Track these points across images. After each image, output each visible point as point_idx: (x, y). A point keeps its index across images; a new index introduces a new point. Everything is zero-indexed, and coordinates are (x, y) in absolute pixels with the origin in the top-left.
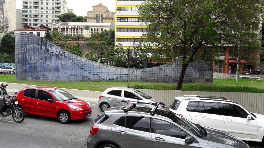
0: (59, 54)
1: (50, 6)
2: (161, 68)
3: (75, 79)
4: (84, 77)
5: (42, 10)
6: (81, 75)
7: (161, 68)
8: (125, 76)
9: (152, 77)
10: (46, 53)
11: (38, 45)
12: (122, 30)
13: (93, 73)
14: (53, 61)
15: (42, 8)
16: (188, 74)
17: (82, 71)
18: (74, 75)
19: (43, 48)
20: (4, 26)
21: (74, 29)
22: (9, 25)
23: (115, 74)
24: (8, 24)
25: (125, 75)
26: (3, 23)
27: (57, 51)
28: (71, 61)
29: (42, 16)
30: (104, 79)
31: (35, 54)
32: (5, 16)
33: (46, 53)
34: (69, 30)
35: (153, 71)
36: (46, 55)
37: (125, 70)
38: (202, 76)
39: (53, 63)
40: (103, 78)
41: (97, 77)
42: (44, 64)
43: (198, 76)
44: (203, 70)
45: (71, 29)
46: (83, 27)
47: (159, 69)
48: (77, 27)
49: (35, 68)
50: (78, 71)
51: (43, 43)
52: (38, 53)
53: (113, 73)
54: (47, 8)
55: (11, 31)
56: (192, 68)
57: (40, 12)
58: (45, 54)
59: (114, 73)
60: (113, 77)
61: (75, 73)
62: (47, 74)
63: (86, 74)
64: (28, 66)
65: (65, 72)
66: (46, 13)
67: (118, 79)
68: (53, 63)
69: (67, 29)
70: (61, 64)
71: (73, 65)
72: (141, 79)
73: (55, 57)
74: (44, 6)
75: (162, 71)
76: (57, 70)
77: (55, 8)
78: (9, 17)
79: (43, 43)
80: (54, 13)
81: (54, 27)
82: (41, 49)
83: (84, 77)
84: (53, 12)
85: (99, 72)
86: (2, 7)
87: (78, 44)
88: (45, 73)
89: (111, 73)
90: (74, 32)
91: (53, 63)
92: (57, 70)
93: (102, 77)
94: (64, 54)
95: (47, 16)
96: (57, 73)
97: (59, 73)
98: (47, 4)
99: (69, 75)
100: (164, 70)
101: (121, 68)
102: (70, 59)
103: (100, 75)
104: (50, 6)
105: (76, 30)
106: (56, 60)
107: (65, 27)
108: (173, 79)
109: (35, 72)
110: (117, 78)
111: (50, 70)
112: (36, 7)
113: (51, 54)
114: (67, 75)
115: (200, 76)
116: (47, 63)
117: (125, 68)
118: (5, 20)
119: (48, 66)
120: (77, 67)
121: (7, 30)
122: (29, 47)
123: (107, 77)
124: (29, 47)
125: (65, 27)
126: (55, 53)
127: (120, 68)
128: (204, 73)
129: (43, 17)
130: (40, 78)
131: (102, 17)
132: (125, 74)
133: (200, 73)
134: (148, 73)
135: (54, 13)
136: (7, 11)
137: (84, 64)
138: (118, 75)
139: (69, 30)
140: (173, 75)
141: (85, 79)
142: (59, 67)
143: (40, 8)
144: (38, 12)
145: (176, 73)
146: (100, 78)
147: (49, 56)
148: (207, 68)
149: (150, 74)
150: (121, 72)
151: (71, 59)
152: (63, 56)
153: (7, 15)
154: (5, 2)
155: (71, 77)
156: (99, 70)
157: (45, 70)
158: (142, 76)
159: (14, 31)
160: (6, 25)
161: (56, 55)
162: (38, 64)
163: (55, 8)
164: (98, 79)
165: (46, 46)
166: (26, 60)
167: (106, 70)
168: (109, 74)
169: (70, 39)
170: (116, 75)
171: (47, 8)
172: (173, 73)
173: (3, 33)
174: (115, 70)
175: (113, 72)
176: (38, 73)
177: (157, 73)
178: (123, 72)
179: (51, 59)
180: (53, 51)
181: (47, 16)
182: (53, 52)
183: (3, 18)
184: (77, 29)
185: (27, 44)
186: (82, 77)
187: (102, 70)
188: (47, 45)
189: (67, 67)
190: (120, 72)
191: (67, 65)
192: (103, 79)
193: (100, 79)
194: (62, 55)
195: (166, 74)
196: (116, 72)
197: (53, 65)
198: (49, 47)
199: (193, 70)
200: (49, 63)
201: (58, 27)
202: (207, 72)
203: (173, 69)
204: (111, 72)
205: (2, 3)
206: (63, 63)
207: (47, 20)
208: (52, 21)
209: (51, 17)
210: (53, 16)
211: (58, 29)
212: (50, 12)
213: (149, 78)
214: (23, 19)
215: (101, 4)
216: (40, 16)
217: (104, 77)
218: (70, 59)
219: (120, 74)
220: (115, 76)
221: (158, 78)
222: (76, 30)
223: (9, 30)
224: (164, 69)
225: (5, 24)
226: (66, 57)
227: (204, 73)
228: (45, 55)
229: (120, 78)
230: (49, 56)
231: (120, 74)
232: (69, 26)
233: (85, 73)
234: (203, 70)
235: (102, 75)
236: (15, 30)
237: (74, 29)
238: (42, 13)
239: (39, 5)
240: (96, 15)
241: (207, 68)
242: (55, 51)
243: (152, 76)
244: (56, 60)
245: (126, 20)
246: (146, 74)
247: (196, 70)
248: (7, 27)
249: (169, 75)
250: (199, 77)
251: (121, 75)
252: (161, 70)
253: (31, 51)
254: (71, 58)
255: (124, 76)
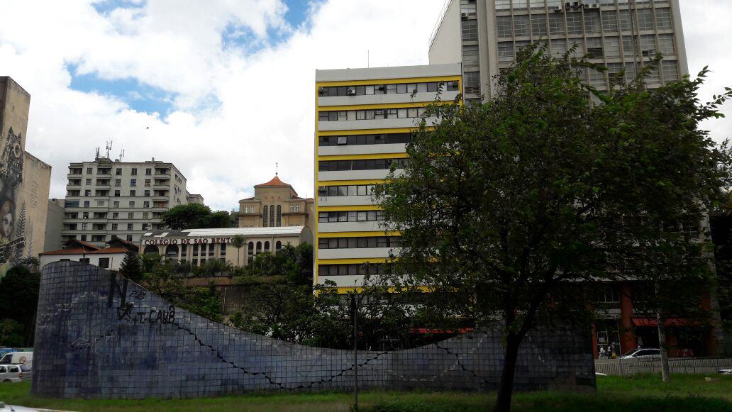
0: (159, 318)
1: (140, 189)
2: (446, 349)
3: (202, 389)
4: (224, 383)
5: (117, 199)
6: (219, 377)
7: (446, 349)
8: (344, 373)
9: (423, 376)
10: (124, 315)
11: (103, 294)
12: (342, 243)
13: (252, 370)
14: (140, 338)
15: (117, 194)
16: (526, 364)
17: (219, 365)
18: (196, 377)
19: (116, 301)
20: (12, 243)
21: (204, 246)
22: (27, 241)
23: (315, 368)
24: (22, 239)
25: (343, 371)
26: (9, 237)
27: (154, 308)
28: (192, 337)
29: (116, 214)
30: (282, 385)
31: (91, 320)
32: (17, 217)
33: (124, 315)
34: (190, 251)
35: (425, 356)
36: (124, 321)
37: (344, 356)
38: (565, 369)
39: (142, 343)
40: (280, 384)
41: (263, 381)
42: (114, 347)
43: (554, 370)
44: (565, 350)
45: (196, 246)
46: (228, 239)
47: (440, 351)
48: (210, 241)
49: (88, 360)
50: (208, 366)
51: (116, 289)
52: (100, 316)
53: (308, 368)
54: (133, 193)
55: (30, 257)
56: (534, 346)
57: (112, 206)
58: (120, 318)
59: (312, 366)
60: (309, 380)
61: (202, 372)
62: (123, 376)
63: (232, 373)
64: (69, 355)
65: (172, 370)
66: (128, 206)
67: (324, 384)
68: (140, 344)
69: (184, 246)
70: (163, 348)
71: (197, 349)
72: (392, 381)
73: (148, 328)
74: (125, 189)
75: (450, 356)
76: (150, 363)
77: (152, 194)
78: (27, 221)
79: (116, 289)
80: (151, 205)
81: (148, 243)
82: (110, 304)
83: (224, 383)
84: (147, 203)
85: (269, 364)
86: (13, 194)
87: (213, 287)
88: (116, 373)
89: (303, 368)
90: (203, 255)
91: (142, 343)
92: (150, 363)
93: (278, 381)
94: (172, 316)
95: (131, 215)
96: (149, 372)
97: (156, 372)
98: (133, 182)
99: (184, 378)
100: (457, 355)
101: (333, 350)
102: (188, 330)
103: (273, 376)
104: (140, 189)
105: (208, 248)
106: (149, 336)
107: (179, 242)
108: (483, 381)
109: (87, 371)
110: (320, 383)
111: (131, 366)
112: (103, 193)
113: (135, 320)
114: (178, 378)
115: (559, 370)
116: (123, 343)
117: (344, 352)
118: (16, 227)
119: (126, 353)
120: (208, 354)
121: (18, 254)
122: (75, 300)
123: (293, 380)
124: (75, 300)
125: (179, 242)
126: (147, 316)
127: (329, 350)
128: (569, 361)
129: (120, 216)
130: (100, 388)
131: (279, 211)
132: (344, 368)
133: (559, 360)
134: (410, 362)
135: (151, 205)
136: (24, 205)
137: (226, 342)
138: (324, 374)
139: (190, 251)
140: (481, 368)
141: (230, 388)
142: (157, 355)
143: (112, 193)
144: (106, 205)
145: (492, 362)
146: (271, 383)
147: (131, 324)
148: (577, 345)
149: (416, 368)
150: (334, 363)
151: (192, 331)
152: (169, 322)
153: (22, 214)
154: (21, 181)
155: (190, 383)
156: (269, 359)
157: (116, 366)
158: (395, 374)
159: (35, 255)
160: (18, 241)
161: (150, 320)
162: (97, 348)
163: (152, 194)
164: (268, 386)
165: (123, 296)
166: (65, 338)
167: (289, 358)
168: (299, 369)
169: (191, 274)
170: (319, 374)
171: (133, 193)
172: (481, 362)
173: (8, 262)
174: (315, 357)
175: (309, 363)
176: (96, 374)
177: (435, 362)
178: (339, 363)
179: (135, 334)
180: (142, 310)
181: (131, 215)
182: (141, 314)
183: (12, 224)
184: (212, 246)
185: (71, 294)
186: (220, 382)
187: (279, 358)
188: (128, 294)
189: (179, 356)
190: (329, 363)
191: (179, 349)
192: (282, 388)
193: (274, 386)
194: (166, 322)
195: (462, 366)
196: (319, 363)
197: (140, 349)
198: (132, 298)
199: (536, 351)
200: (129, 344)
201: (158, 242)
202: (577, 357)
203: (481, 351)
204: (304, 363)
205: (14, 185)
206: (169, 344)
207: (130, 226)
208: (144, 226)
209: (140, 216)
210: (145, 214)
211: (160, 249)
212: (139, 203)
213: (414, 379)
214: (65, 225)
215: (276, 179)
216: (110, 216)
217: (283, 381)
218: (188, 330)
219: (329, 368)
220: (315, 375)
221: (439, 377)
222: (208, 248)
223: (25, 255)
224: (455, 351)
225: (16, 238)
226: (177, 324)
227: (569, 361)
228: (118, 324)
229: (330, 380)
230: (131, 324)
231: (329, 368)
232: (188, 240)
233: (230, 371)
234: (565, 350)
235: (279, 375)
236: (40, 255)
237: (204, 246)
238: (117, 207)
239: (112, 187)
240: (262, 208)
241: (577, 345)
242: (149, 310)
243: (421, 372)
244: (149, 336)
245: (343, 218)
246: (406, 368)
247: (547, 351)
248: (21, 246)
249: (470, 368)
250: (558, 373)
251: (334, 373)
252: (449, 353)
253: (81, 312)
254: (192, 327)
255: (341, 375)
